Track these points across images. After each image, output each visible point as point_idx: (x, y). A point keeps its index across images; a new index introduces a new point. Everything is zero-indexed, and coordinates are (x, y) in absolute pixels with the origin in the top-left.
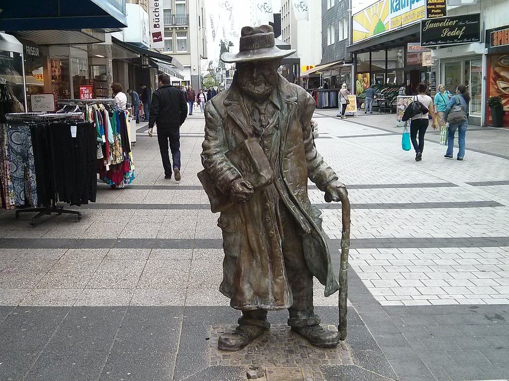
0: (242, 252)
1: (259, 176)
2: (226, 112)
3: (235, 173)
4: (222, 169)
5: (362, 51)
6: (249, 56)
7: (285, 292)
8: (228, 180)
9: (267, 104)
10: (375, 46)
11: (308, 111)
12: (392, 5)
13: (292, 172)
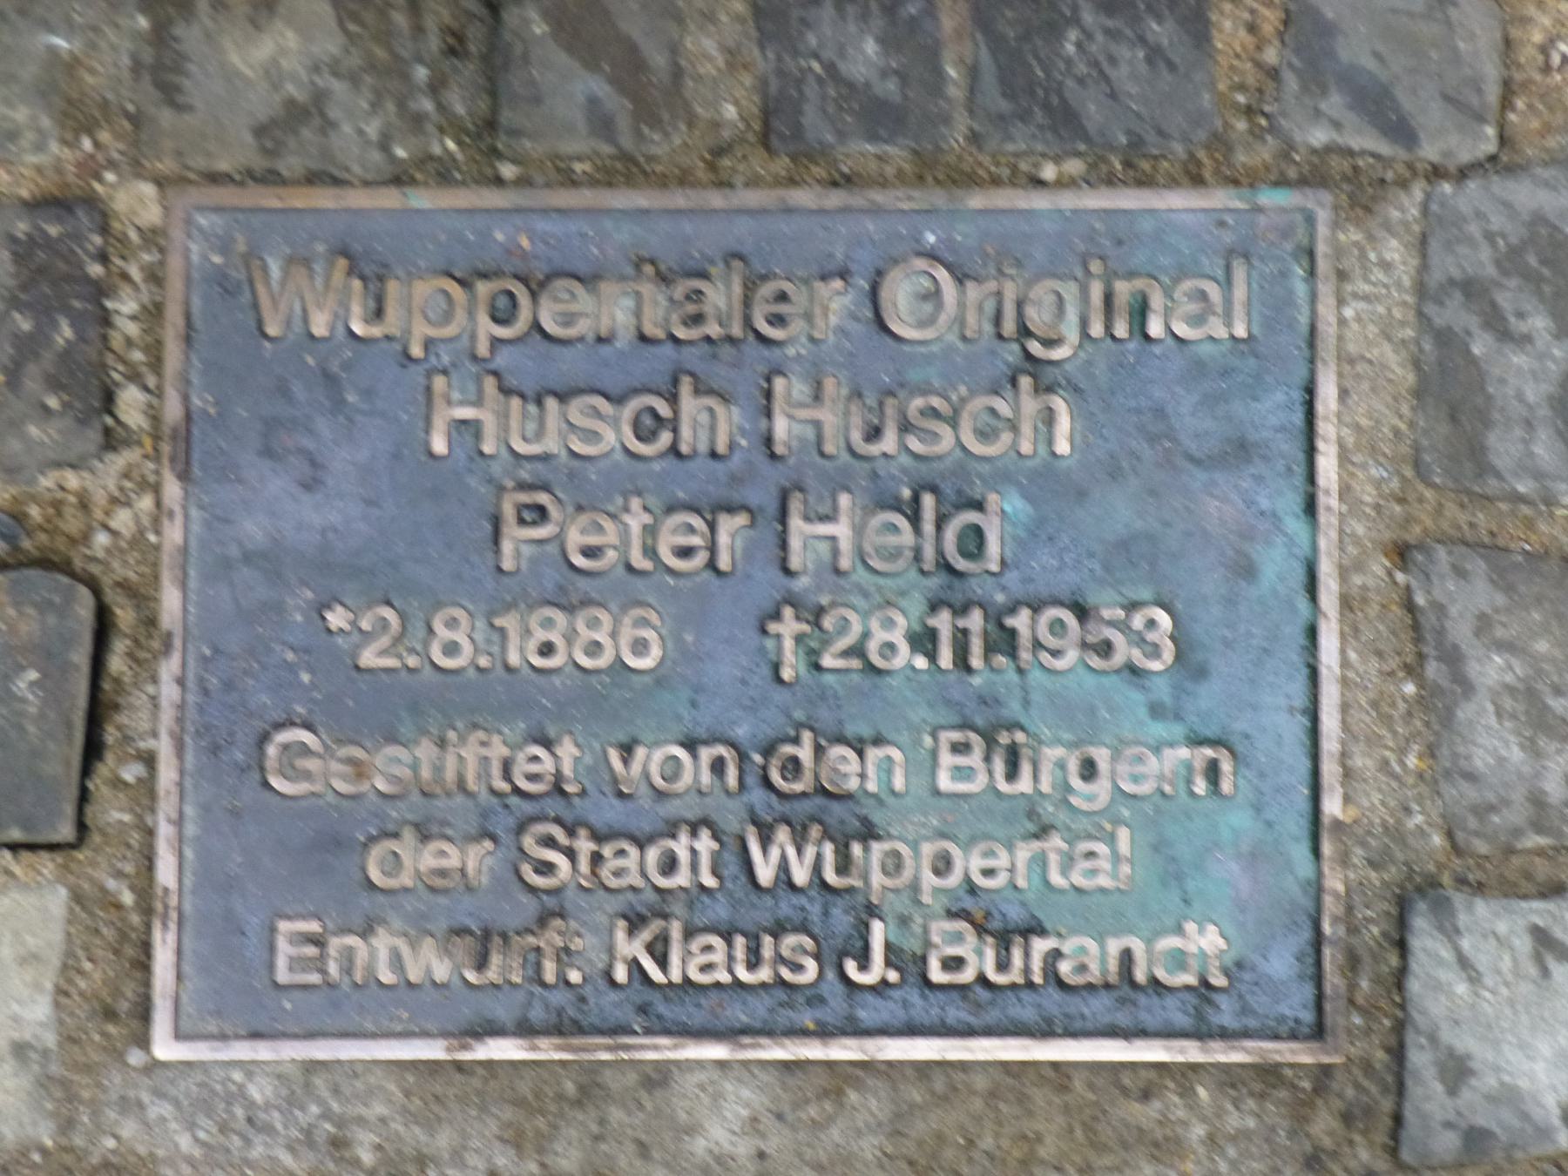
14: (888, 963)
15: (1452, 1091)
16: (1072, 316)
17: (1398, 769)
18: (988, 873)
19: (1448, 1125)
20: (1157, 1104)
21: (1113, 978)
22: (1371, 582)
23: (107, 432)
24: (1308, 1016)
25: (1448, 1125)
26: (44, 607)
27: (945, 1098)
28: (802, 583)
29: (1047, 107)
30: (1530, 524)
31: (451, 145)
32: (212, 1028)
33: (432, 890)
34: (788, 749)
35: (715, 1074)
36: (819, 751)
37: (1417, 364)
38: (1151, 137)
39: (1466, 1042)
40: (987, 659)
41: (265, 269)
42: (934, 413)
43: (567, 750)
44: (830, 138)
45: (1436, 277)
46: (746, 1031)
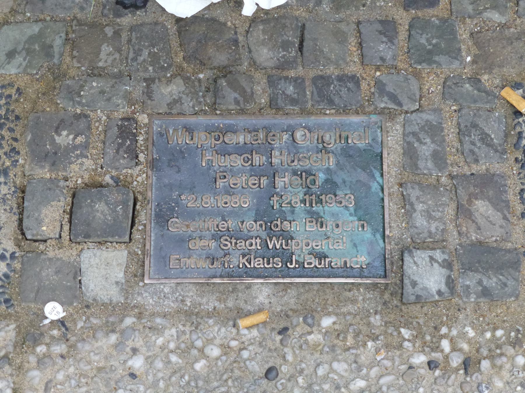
14: (296, 264)
15: (413, 288)
16: (333, 138)
17: (401, 226)
18: (317, 246)
19: (412, 294)
20: (352, 292)
21: (343, 266)
22: (394, 190)
23: (136, 163)
24: (383, 273)
25: (412, 294)
26: (123, 194)
27: (308, 291)
28: (278, 190)
29: (327, 99)
30: (427, 179)
31: (207, 108)
32: (157, 277)
33: (202, 249)
34: (275, 222)
35: (261, 286)
36: (282, 223)
37: (403, 148)
38: (349, 105)
39: (416, 278)
40: (316, 205)
41: (169, 131)
42: (305, 157)
43: (230, 222)
44: (283, 105)
45: (407, 132)
46: (266, 277)
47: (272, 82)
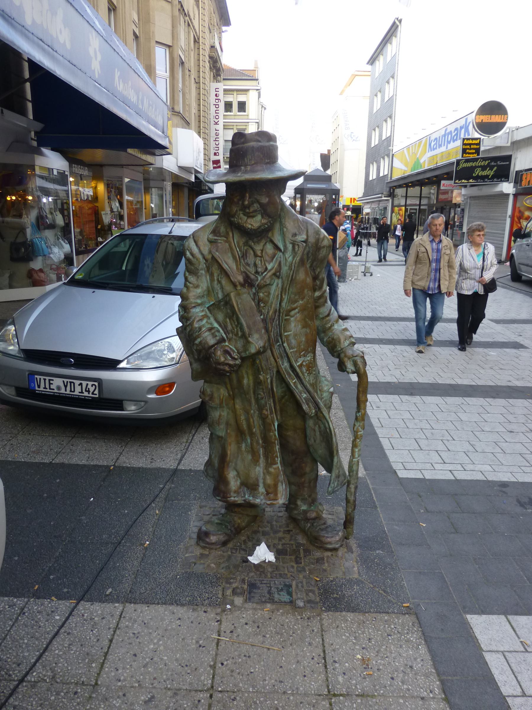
0: (228, 431)
1: (247, 343)
2: (210, 252)
3: (216, 336)
4: (200, 328)
5: (400, 186)
6: (239, 175)
7: (280, 484)
8: (206, 346)
9: (265, 243)
10: (411, 182)
11: (321, 255)
12: (430, 145)
13: (295, 335)
47: (271, 573)
